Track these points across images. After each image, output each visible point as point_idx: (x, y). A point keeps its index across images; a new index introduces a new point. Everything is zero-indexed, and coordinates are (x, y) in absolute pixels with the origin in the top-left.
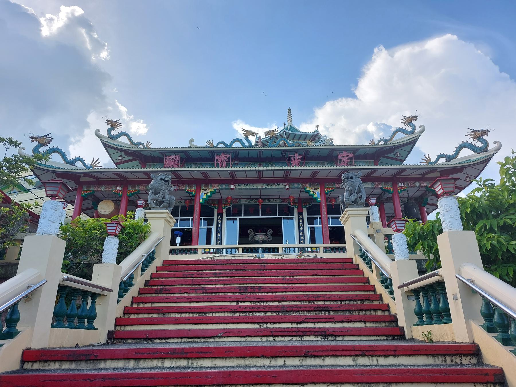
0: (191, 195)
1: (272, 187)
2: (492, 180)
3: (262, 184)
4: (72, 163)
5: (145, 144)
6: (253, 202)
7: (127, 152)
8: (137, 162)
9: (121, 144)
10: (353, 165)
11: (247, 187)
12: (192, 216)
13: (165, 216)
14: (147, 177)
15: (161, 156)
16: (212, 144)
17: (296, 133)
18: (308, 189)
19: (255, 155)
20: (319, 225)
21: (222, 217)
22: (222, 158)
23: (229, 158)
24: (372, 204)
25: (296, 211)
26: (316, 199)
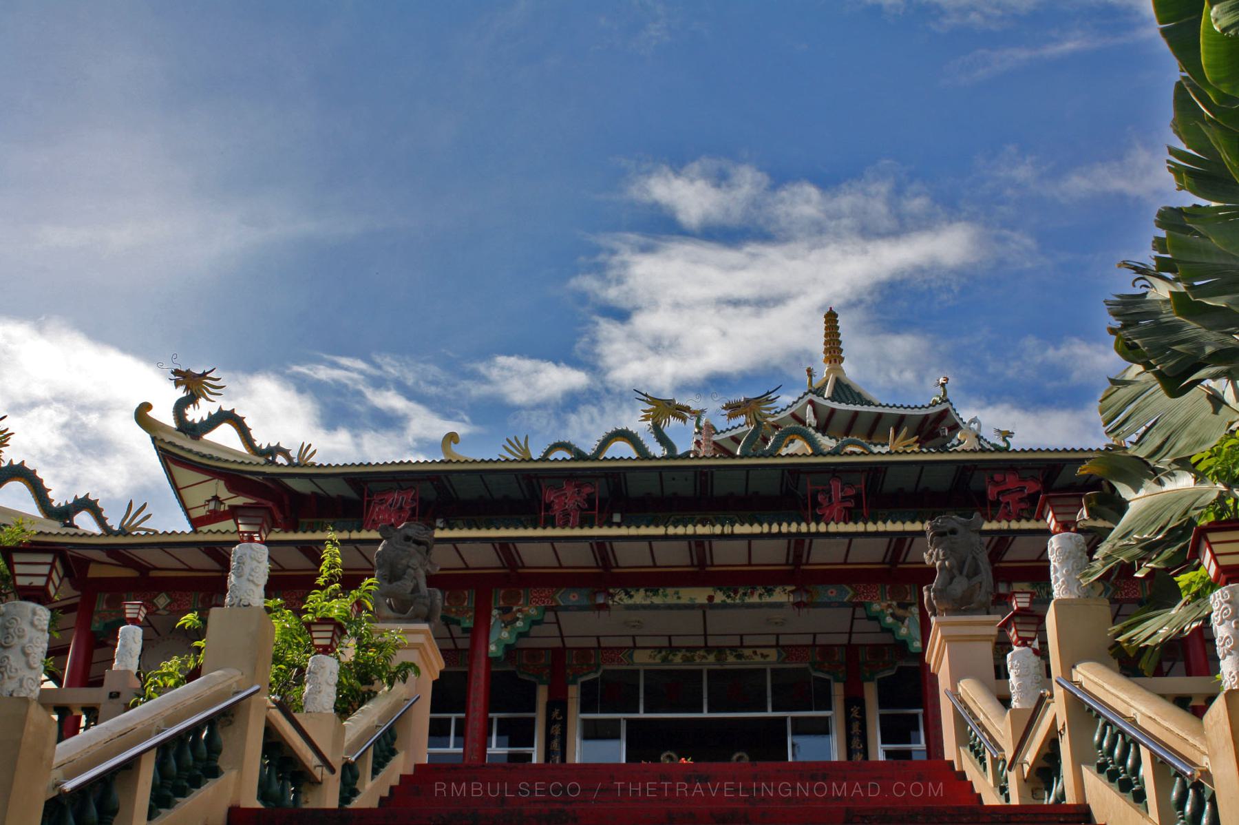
0: (456, 630)
1: (748, 600)
3: (709, 591)
4: (64, 514)
5: (294, 454)
7: (234, 478)
9: (215, 454)
11: (657, 600)
12: (461, 706)
13: (420, 639)
15: (349, 493)
16: (526, 451)
17: (858, 408)
18: (876, 607)
19: (685, 488)
21: (564, 712)
22: (571, 498)
23: (590, 500)
25: (838, 690)
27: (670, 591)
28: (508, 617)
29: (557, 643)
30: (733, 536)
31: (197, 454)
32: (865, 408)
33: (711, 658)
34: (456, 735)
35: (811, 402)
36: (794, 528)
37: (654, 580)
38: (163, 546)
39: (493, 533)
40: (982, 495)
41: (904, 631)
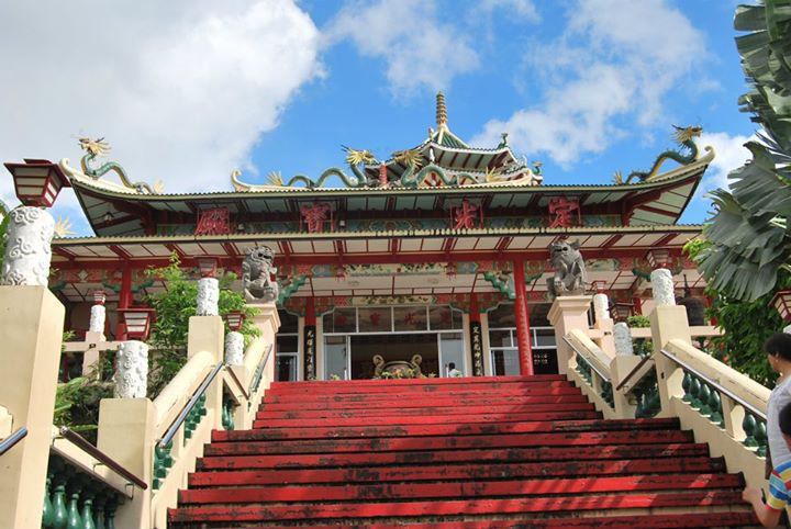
2: (232, 177)
3: (398, 266)
5: (151, 188)
6: (377, 302)
7: (119, 202)
8: (136, 223)
10: (577, 226)
14: (116, 255)
17: (457, 150)
18: (490, 274)
20: (514, 348)
21: (314, 332)
23: (328, 214)
24: (599, 292)
25: (466, 318)
26: (502, 295)
27: (376, 266)
28: (285, 281)
29: (310, 294)
30: (414, 237)
31: (98, 189)
32: (462, 151)
33: (396, 301)
34: (514, 336)
35: (431, 147)
36: (448, 232)
37: (368, 260)
38: (84, 245)
39: (278, 236)
40: (547, 208)
41: (506, 287)
